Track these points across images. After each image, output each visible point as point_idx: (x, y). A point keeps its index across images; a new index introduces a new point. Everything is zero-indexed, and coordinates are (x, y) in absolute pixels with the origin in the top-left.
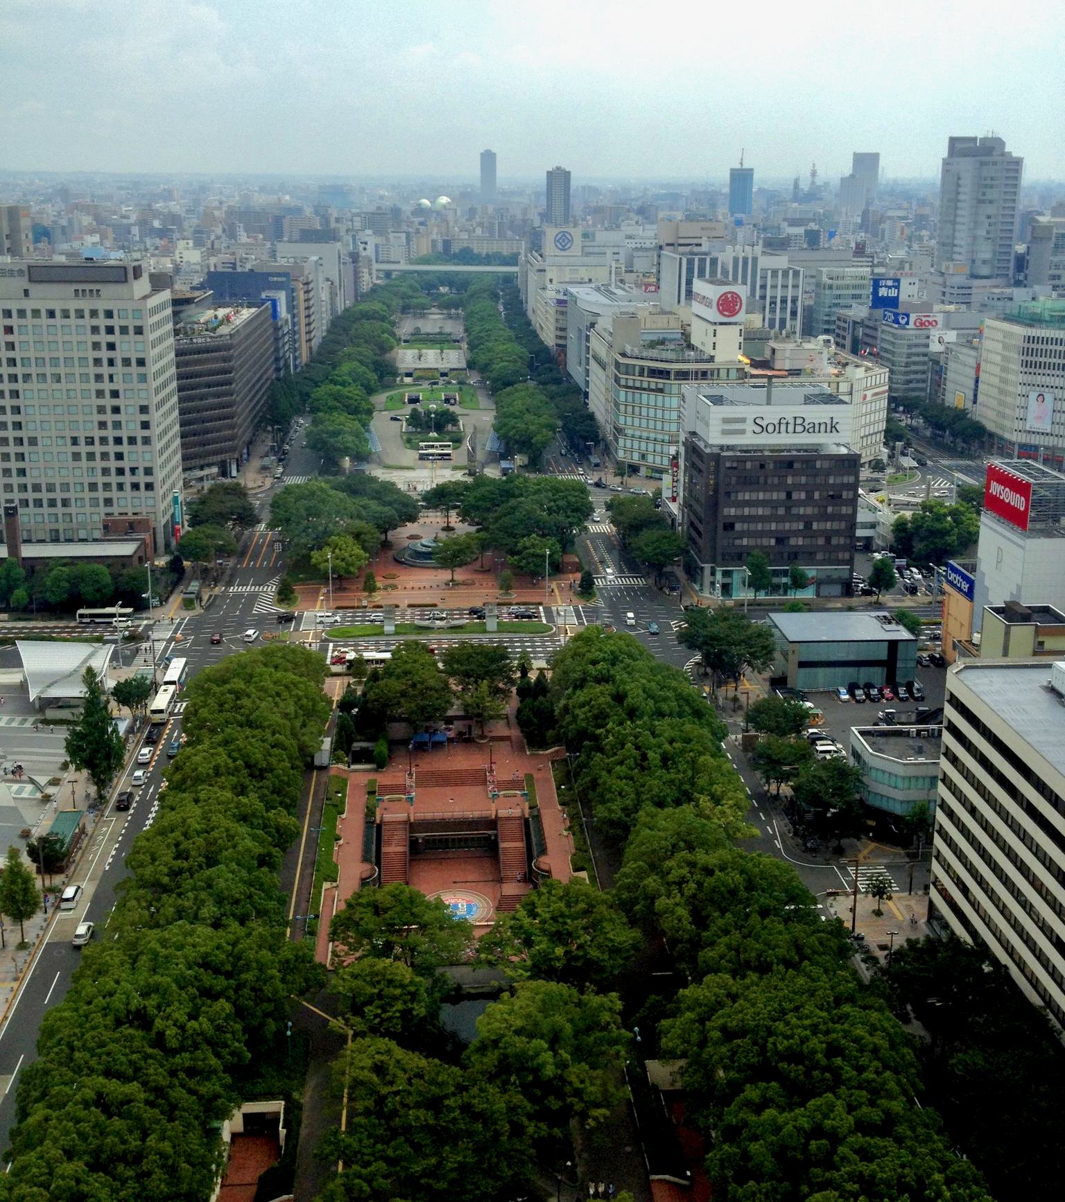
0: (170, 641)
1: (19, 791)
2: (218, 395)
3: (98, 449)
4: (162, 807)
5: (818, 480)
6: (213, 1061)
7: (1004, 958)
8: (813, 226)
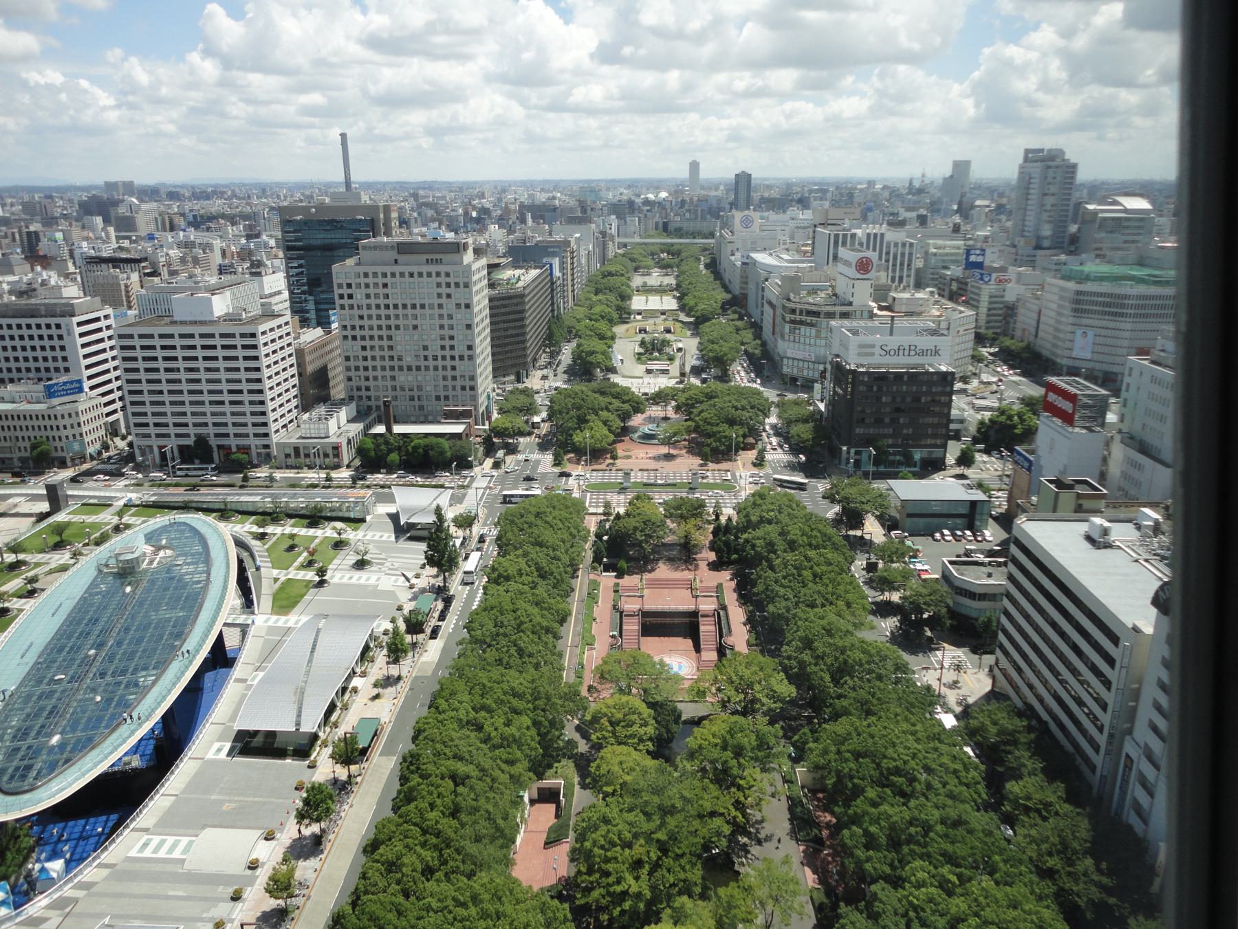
0: (485, 489)
1: (396, 581)
2: (515, 328)
3: (440, 363)
4: (485, 594)
5: (924, 389)
6: (519, 754)
7: (1045, 716)
8: (923, 212)
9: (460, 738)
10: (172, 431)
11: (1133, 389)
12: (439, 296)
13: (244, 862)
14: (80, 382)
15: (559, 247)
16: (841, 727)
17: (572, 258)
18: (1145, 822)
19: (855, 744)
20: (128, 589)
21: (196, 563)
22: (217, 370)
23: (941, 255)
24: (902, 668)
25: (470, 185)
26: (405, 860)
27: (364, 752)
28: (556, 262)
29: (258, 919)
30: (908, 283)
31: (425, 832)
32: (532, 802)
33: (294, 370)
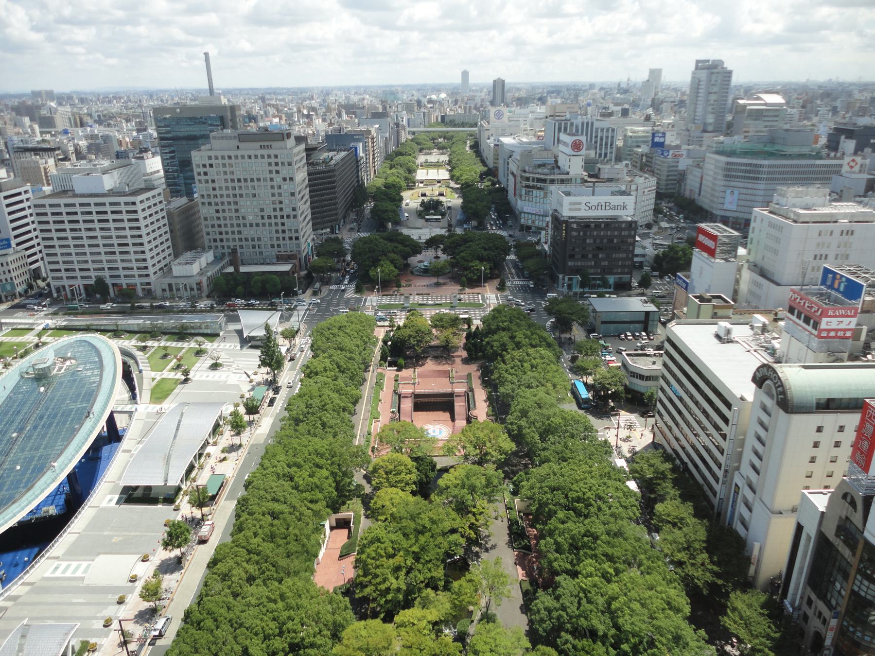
3: (273, 221)
6: (320, 496)
7: (686, 459)
8: (626, 106)
9: (277, 487)
10: (78, 274)
11: (756, 231)
12: (271, 172)
13: (127, 577)
14: (8, 240)
15: (362, 135)
16: (544, 469)
17: (373, 143)
18: (747, 529)
19: (552, 481)
20: (42, 389)
21: (93, 369)
22: (109, 229)
23: (635, 137)
24: (588, 428)
25: (302, 91)
26: (234, 572)
27: (213, 498)
28: (360, 146)
29: (136, 617)
30: (611, 157)
31: (249, 552)
32: (332, 528)
33: (167, 228)
